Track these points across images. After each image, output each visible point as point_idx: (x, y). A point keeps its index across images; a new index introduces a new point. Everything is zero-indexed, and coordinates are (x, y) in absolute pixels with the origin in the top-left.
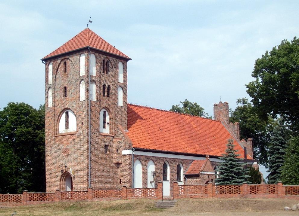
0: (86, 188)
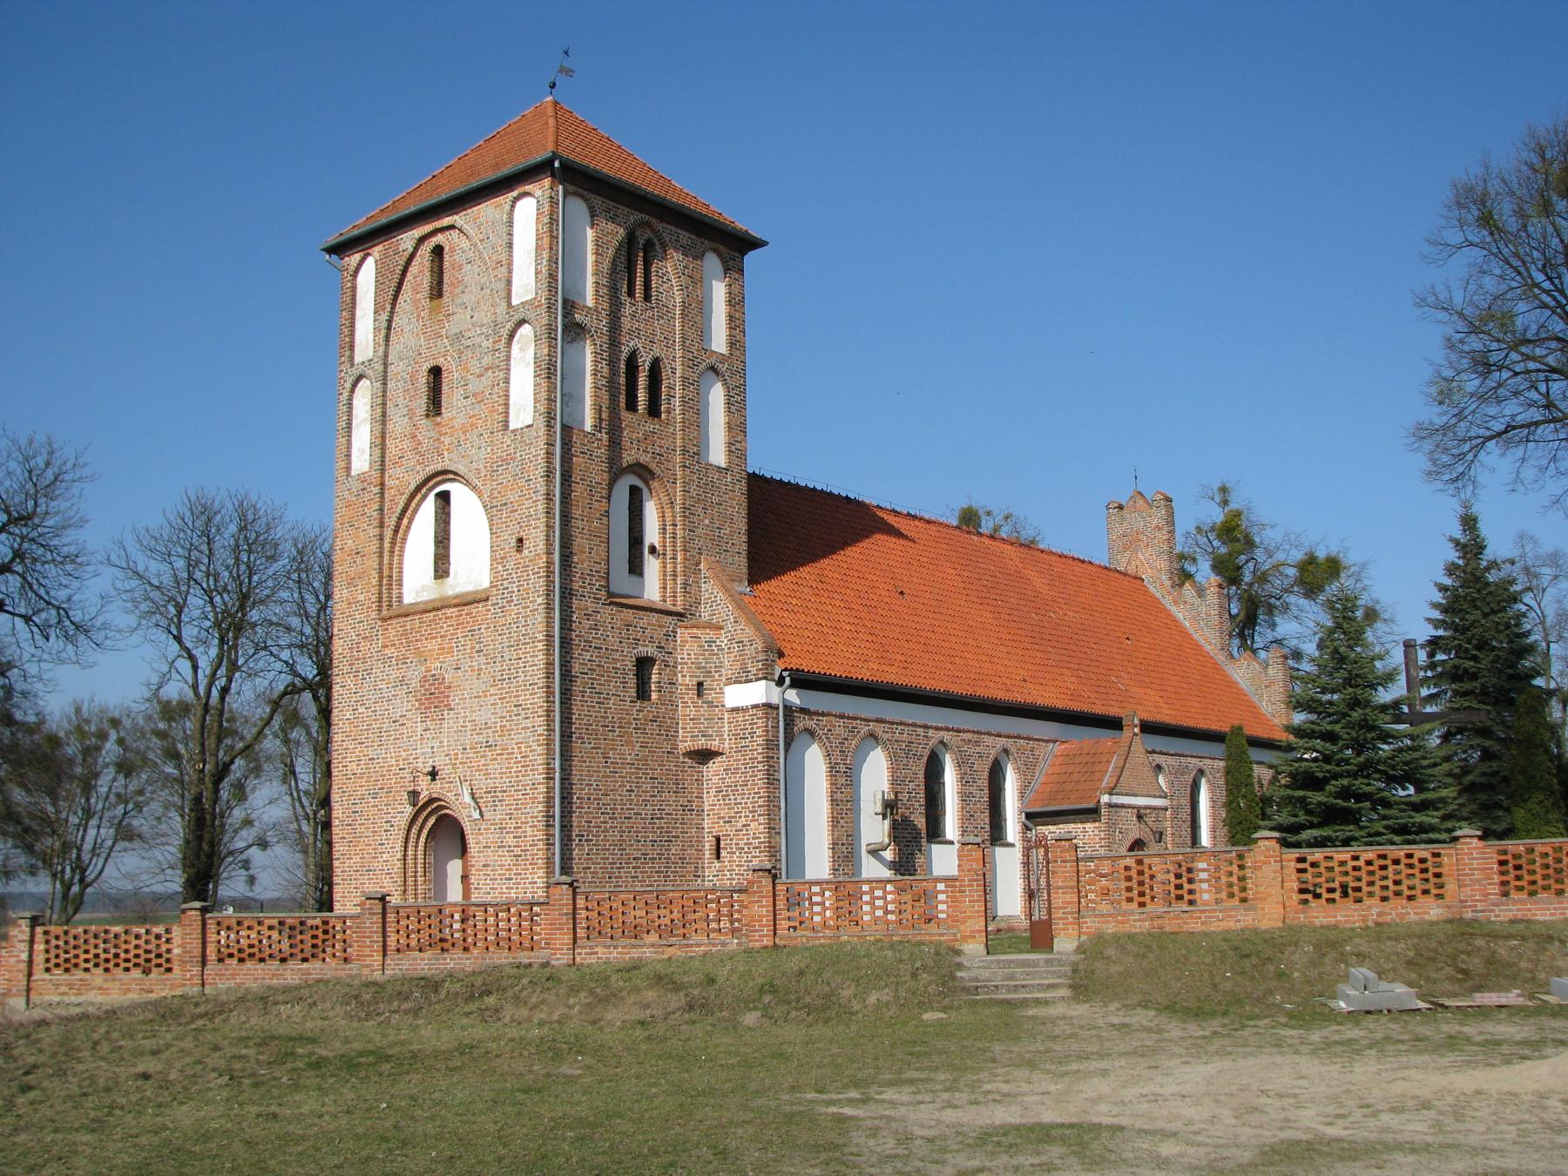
0: (540, 882)
